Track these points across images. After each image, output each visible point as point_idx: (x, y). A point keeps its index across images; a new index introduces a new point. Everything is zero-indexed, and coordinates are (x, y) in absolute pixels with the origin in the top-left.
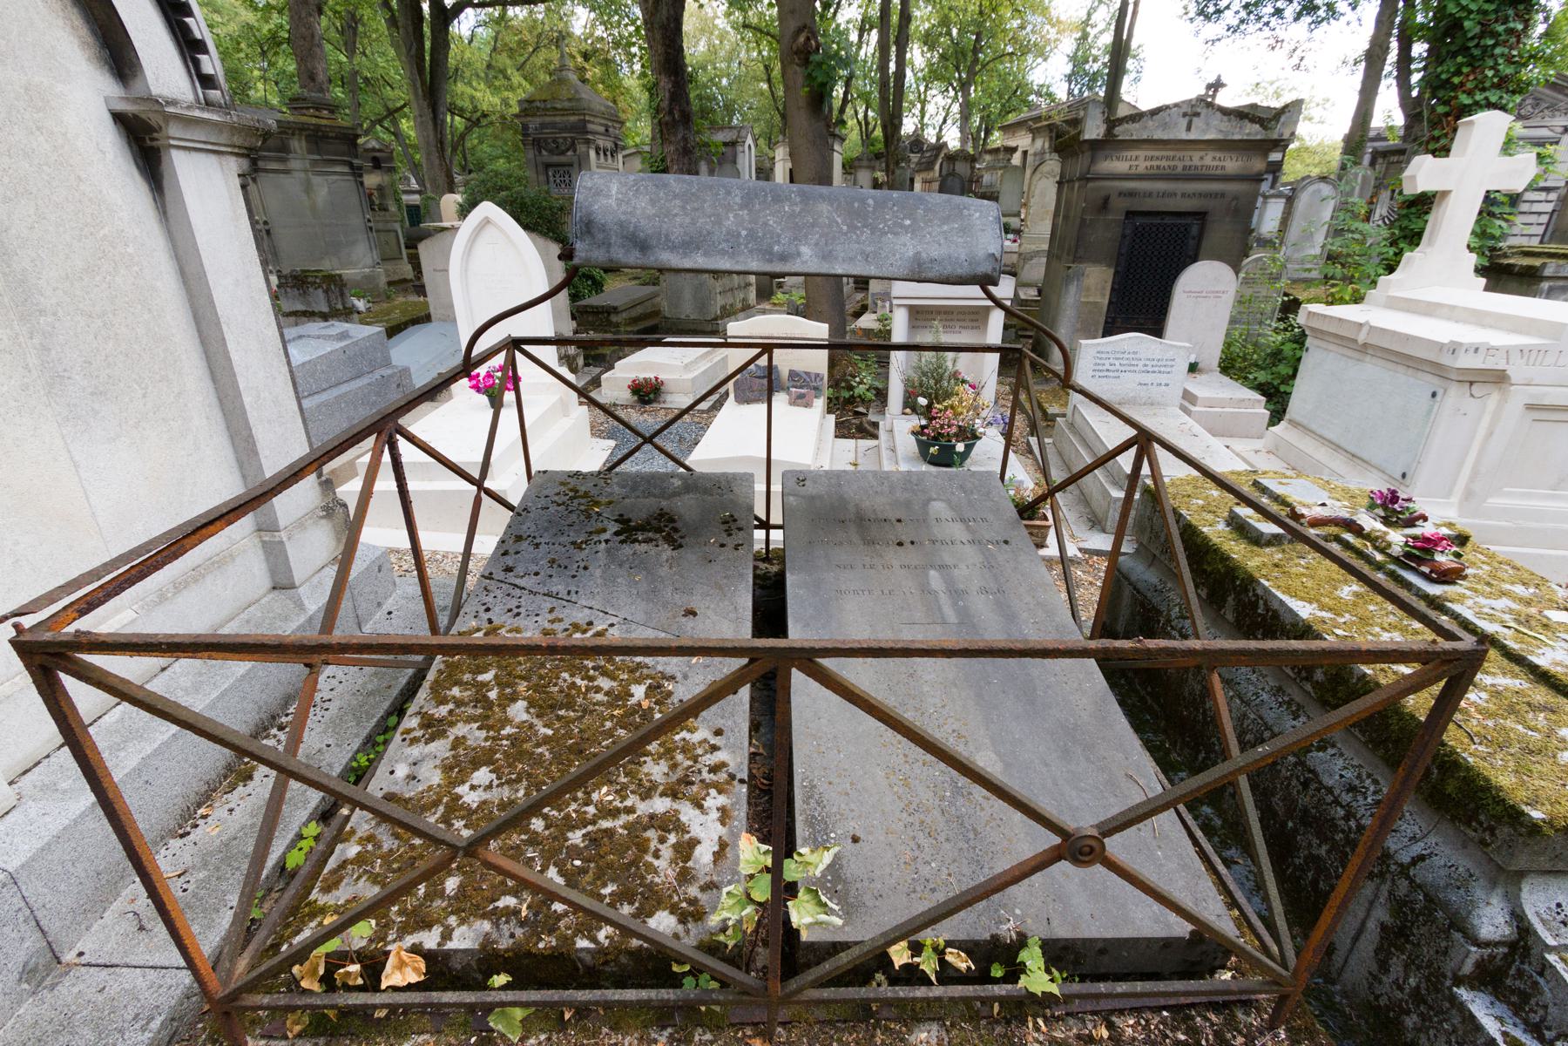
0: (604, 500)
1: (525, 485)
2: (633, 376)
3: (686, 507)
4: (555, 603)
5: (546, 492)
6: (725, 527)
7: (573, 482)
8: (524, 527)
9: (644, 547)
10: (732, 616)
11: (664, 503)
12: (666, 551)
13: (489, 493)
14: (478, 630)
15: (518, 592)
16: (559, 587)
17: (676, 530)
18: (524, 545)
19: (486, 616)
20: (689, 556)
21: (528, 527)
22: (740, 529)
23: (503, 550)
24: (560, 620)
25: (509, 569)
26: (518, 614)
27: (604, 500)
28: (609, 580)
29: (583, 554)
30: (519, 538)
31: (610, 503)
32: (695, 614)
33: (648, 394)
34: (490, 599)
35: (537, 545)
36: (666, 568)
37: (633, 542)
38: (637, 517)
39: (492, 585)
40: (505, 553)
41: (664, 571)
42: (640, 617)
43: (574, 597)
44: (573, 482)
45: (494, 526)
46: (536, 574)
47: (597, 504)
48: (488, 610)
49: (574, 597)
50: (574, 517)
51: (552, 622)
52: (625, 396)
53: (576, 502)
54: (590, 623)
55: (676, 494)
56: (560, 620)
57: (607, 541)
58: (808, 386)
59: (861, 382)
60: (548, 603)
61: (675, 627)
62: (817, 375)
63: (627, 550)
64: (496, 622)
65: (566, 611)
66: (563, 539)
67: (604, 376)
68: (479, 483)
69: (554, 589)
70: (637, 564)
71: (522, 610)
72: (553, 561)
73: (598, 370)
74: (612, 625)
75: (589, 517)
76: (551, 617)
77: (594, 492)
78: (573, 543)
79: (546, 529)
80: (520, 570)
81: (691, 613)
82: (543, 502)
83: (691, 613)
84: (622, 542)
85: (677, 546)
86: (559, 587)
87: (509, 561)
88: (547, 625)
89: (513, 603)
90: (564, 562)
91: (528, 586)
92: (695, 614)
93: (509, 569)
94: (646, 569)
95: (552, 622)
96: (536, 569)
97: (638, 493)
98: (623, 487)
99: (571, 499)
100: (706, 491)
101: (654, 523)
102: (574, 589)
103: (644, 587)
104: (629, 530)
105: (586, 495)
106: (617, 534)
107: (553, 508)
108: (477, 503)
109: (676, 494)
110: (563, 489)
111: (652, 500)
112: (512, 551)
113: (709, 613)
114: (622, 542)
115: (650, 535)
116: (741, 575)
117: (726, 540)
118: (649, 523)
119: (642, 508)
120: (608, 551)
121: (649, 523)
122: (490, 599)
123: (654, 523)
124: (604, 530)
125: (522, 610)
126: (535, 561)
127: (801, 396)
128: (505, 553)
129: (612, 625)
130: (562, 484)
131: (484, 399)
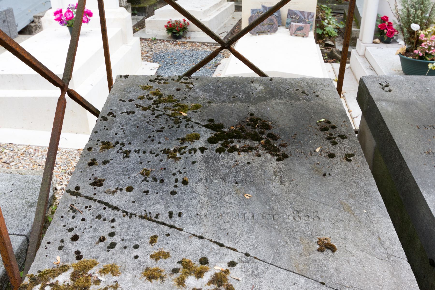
0: (190, 104)
1: (105, 93)
2: (168, 20)
3: (274, 111)
4: (158, 230)
5: (130, 96)
6: (325, 134)
7: (155, 86)
8: (111, 133)
9: (244, 157)
10: (379, 251)
11: (252, 108)
12: (272, 164)
13: (74, 96)
14: (64, 268)
15: (109, 213)
16: (157, 206)
17: (274, 137)
18: (112, 153)
19: (72, 247)
20: (299, 168)
21: (114, 133)
22: (343, 137)
23: (91, 158)
24: (166, 255)
25: (97, 183)
26: (113, 245)
27: (190, 104)
28: (216, 198)
29: (180, 165)
30: (106, 145)
31: (197, 107)
32: (333, 249)
33: (178, 32)
34: (77, 222)
35: (127, 154)
36: (277, 184)
37: (233, 150)
38: (230, 123)
39: (80, 203)
40: (92, 163)
41: (275, 187)
42: (264, 252)
43: (177, 222)
44: (155, 86)
45: (78, 133)
46: (130, 189)
47: (183, 108)
48: (75, 238)
49: (177, 222)
50: (161, 122)
51: (156, 257)
52: (163, 33)
53: (162, 106)
54: (204, 261)
55: (261, 99)
56: (166, 255)
57: (202, 150)
58: (305, 22)
59: (329, 23)
60: (148, 230)
61: (313, 267)
62: (309, 14)
63: (227, 159)
64: (87, 257)
65: (172, 241)
66: (154, 146)
67: (146, 20)
68: (62, 83)
69: (153, 210)
70: (242, 179)
71: (117, 239)
72: (145, 173)
73: (141, 18)
74: (232, 264)
75: (177, 122)
76: (154, 250)
77: (178, 96)
78: (166, 151)
79: (134, 135)
80: (110, 184)
81: (326, 246)
82: (127, 106)
83: (326, 246)
84: (219, 151)
85: (282, 157)
86: (157, 206)
87: (98, 172)
88: (151, 263)
89: (104, 229)
90: (159, 175)
91: (121, 206)
92: (333, 249)
93: (97, 183)
94: (254, 183)
95: (156, 257)
96: (128, 182)
97: (223, 98)
98: (206, 91)
99: (155, 102)
100: (291, 96)
101: (248, 129)
102: (176, 210)
103: (258, 207)
104: (224, 137)
105: (170, 99)
106: (211, 141)
107: (139, 113)
108: (61, 105)
109: (261, 99)
110: (146, 92)
111: (238, 105)
112: (99, 161)
113: (350, 247)
114: (219, 151)
115: (248, 142)
116: (367, 193)
117: (333, 150)
118: (242, 129)
119: (232, 114)
120: (206, 161)
121: (242, 129)
122: (77, 222)
123: (248, 129)
124: (197, 137)
125: (117, 239)
126: (126, 172)
127: (300, 29)
128: (92, 163)
129: (232, 264)
130: (145, 88)
131: (65, 30)
